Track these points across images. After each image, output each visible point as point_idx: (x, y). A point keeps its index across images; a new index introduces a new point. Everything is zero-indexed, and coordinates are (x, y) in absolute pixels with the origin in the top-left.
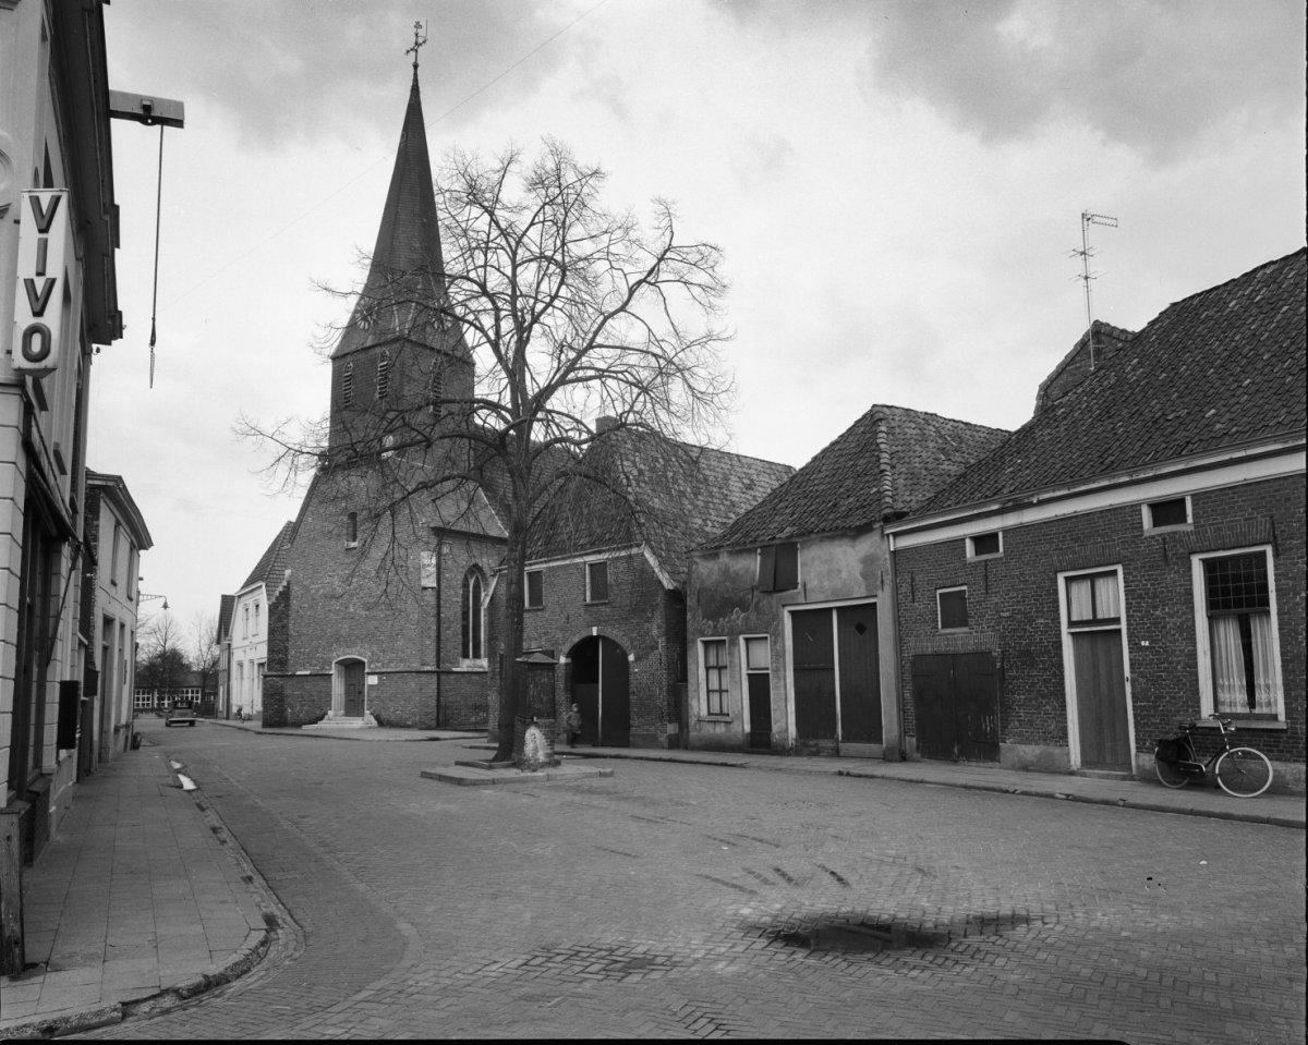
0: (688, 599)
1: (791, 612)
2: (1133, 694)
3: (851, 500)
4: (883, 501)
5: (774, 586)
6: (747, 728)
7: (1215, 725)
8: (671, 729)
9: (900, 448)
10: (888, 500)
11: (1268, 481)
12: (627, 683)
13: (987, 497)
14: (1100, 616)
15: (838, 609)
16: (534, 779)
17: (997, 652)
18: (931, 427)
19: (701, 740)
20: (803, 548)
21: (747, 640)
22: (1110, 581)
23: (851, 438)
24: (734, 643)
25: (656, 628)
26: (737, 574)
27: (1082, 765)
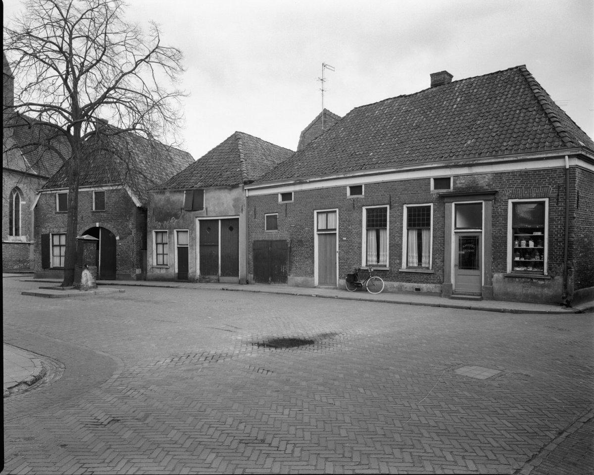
0: (148, 212)
1: (200, 220)
2: (339, 258)
3: (228, 173)
4: (243, 175)
5: (192, 208)
6: (177, 271)
7: (367, 269)
8: (138, 271)
9: (247, 152)
10: (245, 174)
11: (393, 182)
12: (115, 250)
13: (288, 178)
14: (329, 228)
15: (221, 220)
16: (89, 294)
17: (289, 240)
18: (258, 144)
19: (153, 276)
20: (206, 192)
21: (178, 232)
22: (333, 215)
23: (226, 145)
24: (171, 233)
25: (131, 225)
26: (174, 202)
27: (319, 284)
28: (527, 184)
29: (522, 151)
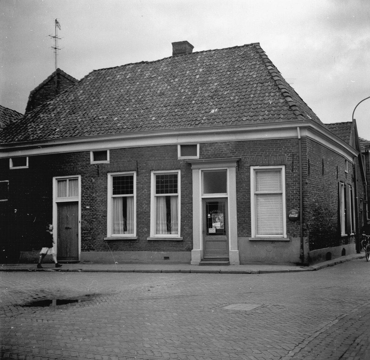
2: (82, 228)
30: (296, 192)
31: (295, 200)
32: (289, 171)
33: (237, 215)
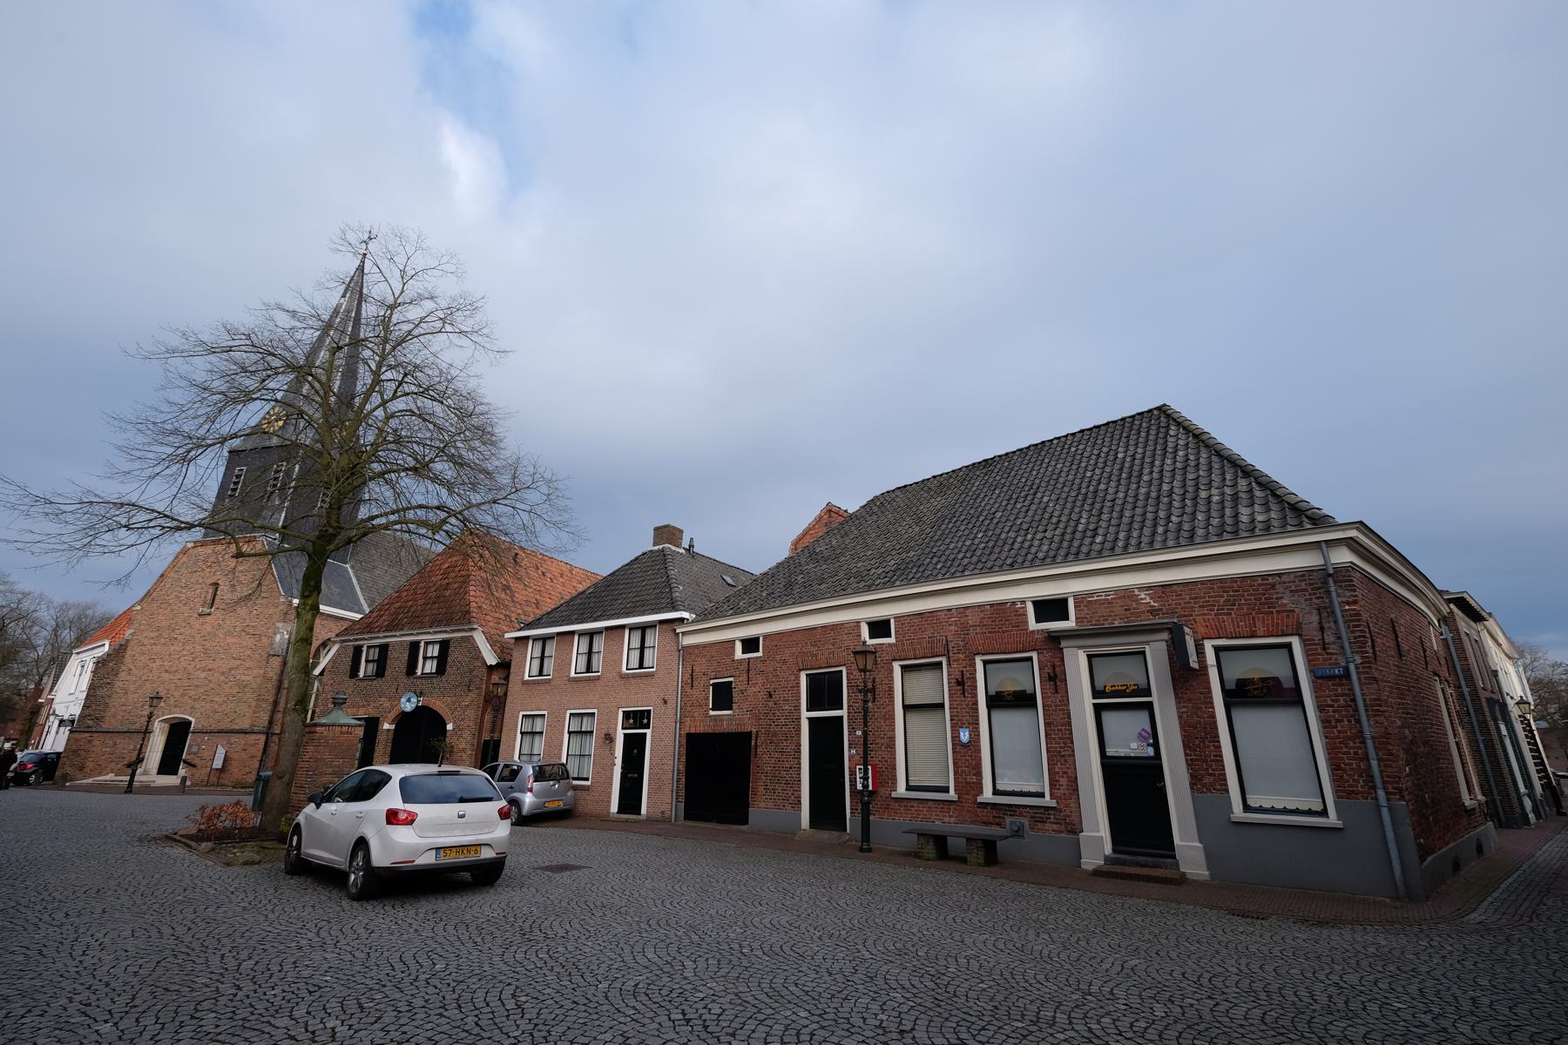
28: (1239, 604)
29: (1215, 538)
30: (1345, 700)
31: (1346, 723)
32: (1316, 649)
33: (1186, 755)
